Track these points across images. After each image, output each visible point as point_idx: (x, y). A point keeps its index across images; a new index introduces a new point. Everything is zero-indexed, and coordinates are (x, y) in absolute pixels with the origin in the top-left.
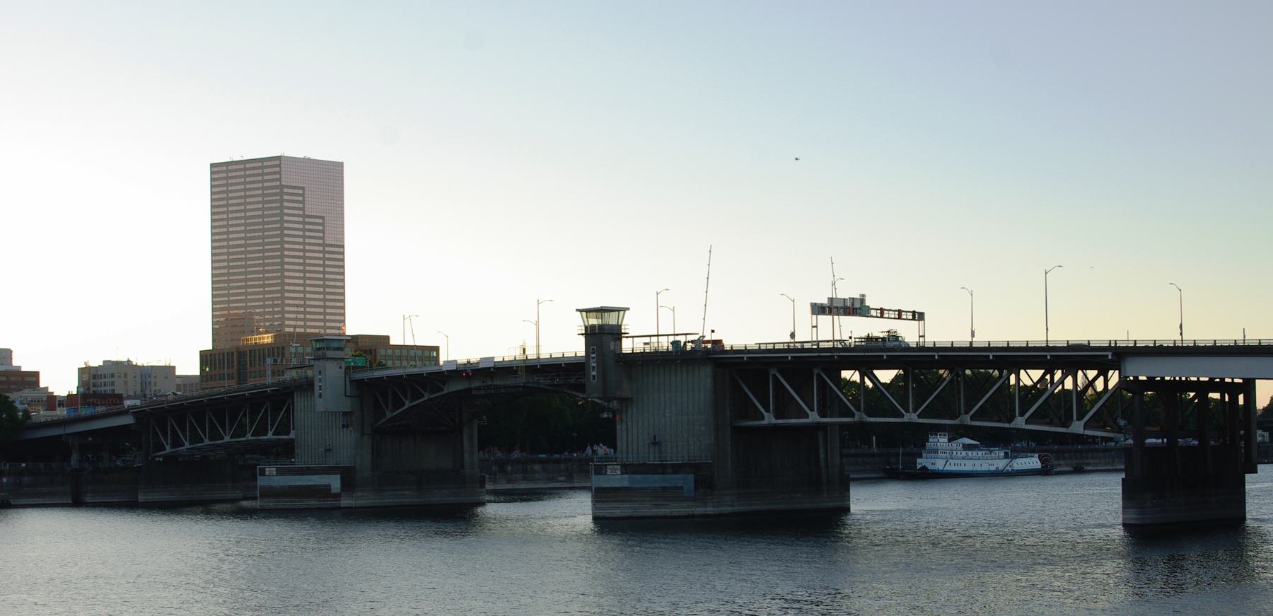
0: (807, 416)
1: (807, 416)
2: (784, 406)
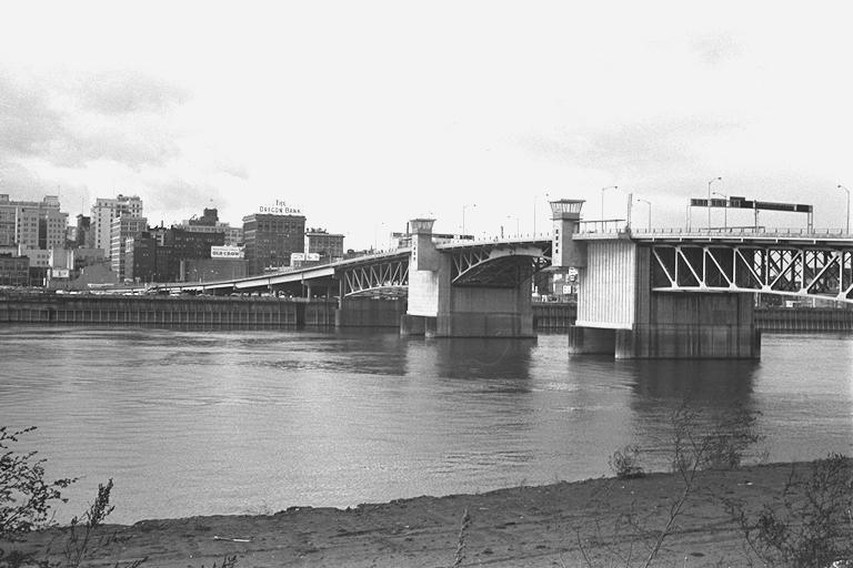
0: (698, 285)
1: (698, 285)
2: (686, 279)
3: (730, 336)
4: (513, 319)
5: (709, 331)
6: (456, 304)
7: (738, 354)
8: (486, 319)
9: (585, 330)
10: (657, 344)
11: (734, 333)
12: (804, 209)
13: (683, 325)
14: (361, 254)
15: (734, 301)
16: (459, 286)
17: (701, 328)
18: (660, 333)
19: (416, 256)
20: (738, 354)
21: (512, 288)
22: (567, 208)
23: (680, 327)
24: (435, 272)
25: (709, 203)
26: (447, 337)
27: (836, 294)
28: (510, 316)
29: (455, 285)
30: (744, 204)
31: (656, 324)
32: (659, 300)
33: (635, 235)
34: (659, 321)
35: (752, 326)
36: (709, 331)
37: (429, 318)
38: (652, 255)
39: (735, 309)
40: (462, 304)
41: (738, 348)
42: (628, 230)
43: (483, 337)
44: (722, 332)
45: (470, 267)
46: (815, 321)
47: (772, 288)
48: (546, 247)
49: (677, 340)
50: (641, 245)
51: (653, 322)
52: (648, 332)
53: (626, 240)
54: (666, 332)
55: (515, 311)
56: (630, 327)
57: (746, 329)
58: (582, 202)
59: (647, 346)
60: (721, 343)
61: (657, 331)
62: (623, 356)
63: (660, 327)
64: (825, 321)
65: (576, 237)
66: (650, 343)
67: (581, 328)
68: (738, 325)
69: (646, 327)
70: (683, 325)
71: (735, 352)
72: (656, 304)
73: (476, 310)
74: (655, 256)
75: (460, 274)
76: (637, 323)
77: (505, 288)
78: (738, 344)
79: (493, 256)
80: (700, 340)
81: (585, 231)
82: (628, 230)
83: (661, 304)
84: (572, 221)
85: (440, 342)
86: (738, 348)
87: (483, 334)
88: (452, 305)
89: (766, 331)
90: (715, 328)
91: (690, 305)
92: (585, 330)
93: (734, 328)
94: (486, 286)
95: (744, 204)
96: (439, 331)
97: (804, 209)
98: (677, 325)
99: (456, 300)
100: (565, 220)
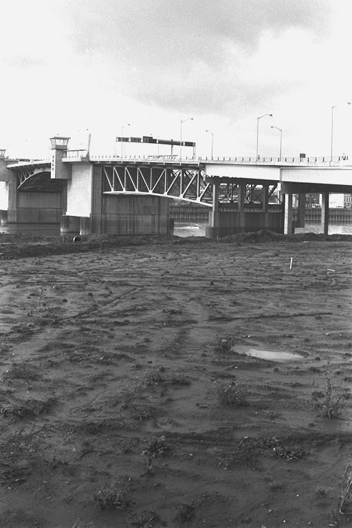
2: (118, 188)
3: (153, 222)
4: (57, 212)
5: (140, 218)
6: (20, 202)
7: (159, 232)
8: (40, 211)
9: (71, 218)
10: (106, 225)
11: (156, 220)
12: (189, 144)
13: (123, 214)
14: (16, 162)
15: (156, 200)
16: (20, 191)
17: (135, 216)
18: (108, 219)
19: (54, 167)
20: (159, 232)
21: (57, 192)
22: (59, 143)
23: (121, 216)
24: (7, 182)
25: (130, 140)
26: (15, 223)
27: (178, 196)
28: (55, 210)
29: (19, 191)
30: (150, 140)
31: (105, 214)
32: (108, 199)
33: (91, 159)
34: (108, 212)
35: (168, 216)
36: (140, 218)
37: (3, 211)
38: (103, 172)
39: (157, 205)
40: (24, 202)
41: (159, 229)
42: (88, 156)
43: (38, 223)
44: (148, 219)
45: (26, 179)
46: (344, 216)
47: (168, 194)
48: (48, 165)
49: (119, 224)
50: (94, 164)
51: (103, 212)
52: (100, 219)
53: (86, 162)
54: (112, 219)
55: (58, 207)
56: (89, 216)
57: (164, 217)
58: (68, 139)
59: (99, 227)
60: (147, 226)
61: (106, 218)
62: (65, 231)
63: (108, 216)
64: (316, 216)
65: (64, 160)
66: (101, 225)
67: (68, 216)
68: (159, 215)
69: (99, 216)
70: (123, 214)
71: (156, 231)
72: (106, 201)
73: (33, 207)
74: (104, 171)
75: (26, 179)
76: (92, 214)
77: (52, 192)
78: (159, 226)
79: (36, 172)
80: (134, 224)
81: (71, 157)
82: (88, 156)
83: (109, 202)
84: (61, 150)
85: (8, 225)
86: (159, 229)
87: (37, 221)
88: (17, 203)
89: (178, 220)
90: (144, 216)
91: (128, 203)
92: (71, 218)
93: (157, 217)
94: (40, 192)
95: (150, 140)
96: (9, 219)
97: (189, 144)
98: (118, 214)
99: (20, 200)
100: (57, 149)
